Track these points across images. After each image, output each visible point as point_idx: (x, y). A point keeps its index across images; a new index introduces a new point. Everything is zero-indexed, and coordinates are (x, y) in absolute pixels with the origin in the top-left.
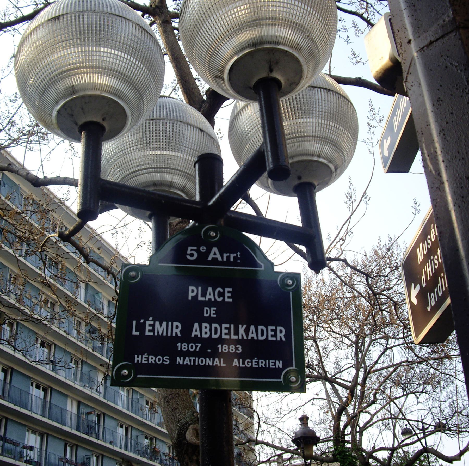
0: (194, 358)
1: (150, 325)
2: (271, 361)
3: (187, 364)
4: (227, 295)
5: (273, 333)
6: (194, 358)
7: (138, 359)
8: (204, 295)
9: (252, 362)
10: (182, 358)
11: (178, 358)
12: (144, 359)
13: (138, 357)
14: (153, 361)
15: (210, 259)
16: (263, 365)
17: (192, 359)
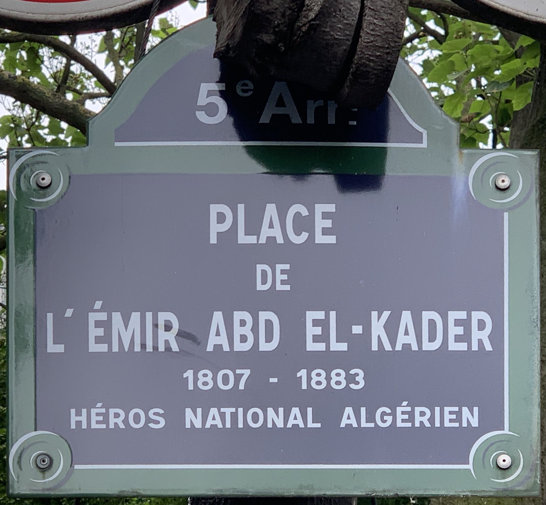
0: (233, 410)
1: (98, 324)
2: (447, 409)
3: (214, 426)
4: (321, 223)
5: (460, 331)
6: (233, 410)
7: (79, 418)
8: (253, 228)
9: (393, 414)
10: (281, 410)
11: (188, 412)
12: (94, 418)
13: (79, 414)
14: (119, 421)
15: (265, 119)
16: (425, 419)
17: (228, 411)
